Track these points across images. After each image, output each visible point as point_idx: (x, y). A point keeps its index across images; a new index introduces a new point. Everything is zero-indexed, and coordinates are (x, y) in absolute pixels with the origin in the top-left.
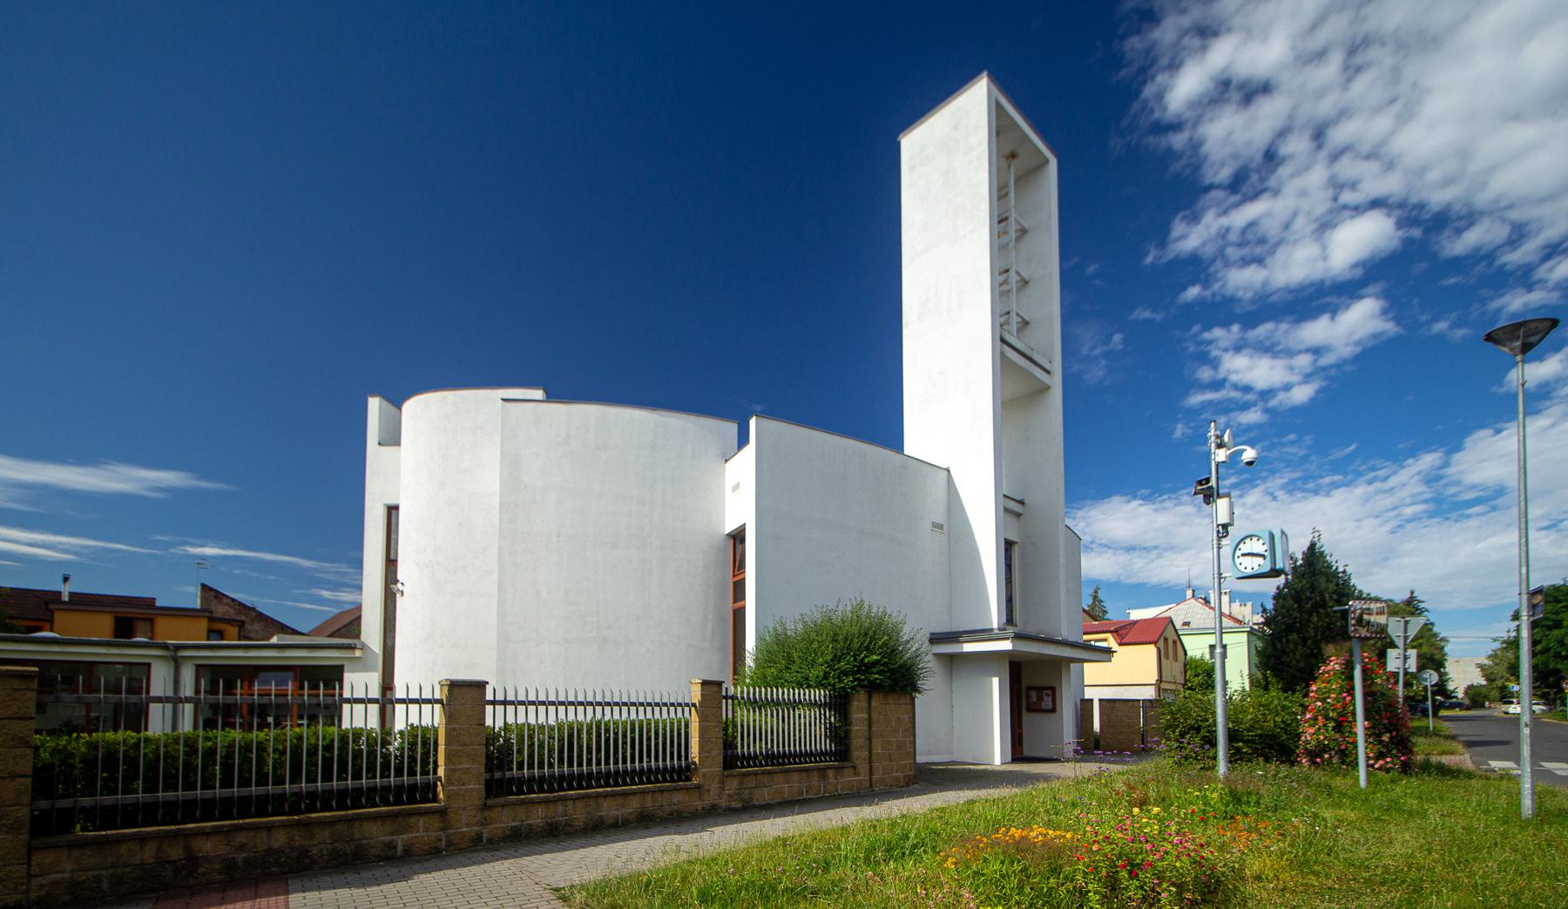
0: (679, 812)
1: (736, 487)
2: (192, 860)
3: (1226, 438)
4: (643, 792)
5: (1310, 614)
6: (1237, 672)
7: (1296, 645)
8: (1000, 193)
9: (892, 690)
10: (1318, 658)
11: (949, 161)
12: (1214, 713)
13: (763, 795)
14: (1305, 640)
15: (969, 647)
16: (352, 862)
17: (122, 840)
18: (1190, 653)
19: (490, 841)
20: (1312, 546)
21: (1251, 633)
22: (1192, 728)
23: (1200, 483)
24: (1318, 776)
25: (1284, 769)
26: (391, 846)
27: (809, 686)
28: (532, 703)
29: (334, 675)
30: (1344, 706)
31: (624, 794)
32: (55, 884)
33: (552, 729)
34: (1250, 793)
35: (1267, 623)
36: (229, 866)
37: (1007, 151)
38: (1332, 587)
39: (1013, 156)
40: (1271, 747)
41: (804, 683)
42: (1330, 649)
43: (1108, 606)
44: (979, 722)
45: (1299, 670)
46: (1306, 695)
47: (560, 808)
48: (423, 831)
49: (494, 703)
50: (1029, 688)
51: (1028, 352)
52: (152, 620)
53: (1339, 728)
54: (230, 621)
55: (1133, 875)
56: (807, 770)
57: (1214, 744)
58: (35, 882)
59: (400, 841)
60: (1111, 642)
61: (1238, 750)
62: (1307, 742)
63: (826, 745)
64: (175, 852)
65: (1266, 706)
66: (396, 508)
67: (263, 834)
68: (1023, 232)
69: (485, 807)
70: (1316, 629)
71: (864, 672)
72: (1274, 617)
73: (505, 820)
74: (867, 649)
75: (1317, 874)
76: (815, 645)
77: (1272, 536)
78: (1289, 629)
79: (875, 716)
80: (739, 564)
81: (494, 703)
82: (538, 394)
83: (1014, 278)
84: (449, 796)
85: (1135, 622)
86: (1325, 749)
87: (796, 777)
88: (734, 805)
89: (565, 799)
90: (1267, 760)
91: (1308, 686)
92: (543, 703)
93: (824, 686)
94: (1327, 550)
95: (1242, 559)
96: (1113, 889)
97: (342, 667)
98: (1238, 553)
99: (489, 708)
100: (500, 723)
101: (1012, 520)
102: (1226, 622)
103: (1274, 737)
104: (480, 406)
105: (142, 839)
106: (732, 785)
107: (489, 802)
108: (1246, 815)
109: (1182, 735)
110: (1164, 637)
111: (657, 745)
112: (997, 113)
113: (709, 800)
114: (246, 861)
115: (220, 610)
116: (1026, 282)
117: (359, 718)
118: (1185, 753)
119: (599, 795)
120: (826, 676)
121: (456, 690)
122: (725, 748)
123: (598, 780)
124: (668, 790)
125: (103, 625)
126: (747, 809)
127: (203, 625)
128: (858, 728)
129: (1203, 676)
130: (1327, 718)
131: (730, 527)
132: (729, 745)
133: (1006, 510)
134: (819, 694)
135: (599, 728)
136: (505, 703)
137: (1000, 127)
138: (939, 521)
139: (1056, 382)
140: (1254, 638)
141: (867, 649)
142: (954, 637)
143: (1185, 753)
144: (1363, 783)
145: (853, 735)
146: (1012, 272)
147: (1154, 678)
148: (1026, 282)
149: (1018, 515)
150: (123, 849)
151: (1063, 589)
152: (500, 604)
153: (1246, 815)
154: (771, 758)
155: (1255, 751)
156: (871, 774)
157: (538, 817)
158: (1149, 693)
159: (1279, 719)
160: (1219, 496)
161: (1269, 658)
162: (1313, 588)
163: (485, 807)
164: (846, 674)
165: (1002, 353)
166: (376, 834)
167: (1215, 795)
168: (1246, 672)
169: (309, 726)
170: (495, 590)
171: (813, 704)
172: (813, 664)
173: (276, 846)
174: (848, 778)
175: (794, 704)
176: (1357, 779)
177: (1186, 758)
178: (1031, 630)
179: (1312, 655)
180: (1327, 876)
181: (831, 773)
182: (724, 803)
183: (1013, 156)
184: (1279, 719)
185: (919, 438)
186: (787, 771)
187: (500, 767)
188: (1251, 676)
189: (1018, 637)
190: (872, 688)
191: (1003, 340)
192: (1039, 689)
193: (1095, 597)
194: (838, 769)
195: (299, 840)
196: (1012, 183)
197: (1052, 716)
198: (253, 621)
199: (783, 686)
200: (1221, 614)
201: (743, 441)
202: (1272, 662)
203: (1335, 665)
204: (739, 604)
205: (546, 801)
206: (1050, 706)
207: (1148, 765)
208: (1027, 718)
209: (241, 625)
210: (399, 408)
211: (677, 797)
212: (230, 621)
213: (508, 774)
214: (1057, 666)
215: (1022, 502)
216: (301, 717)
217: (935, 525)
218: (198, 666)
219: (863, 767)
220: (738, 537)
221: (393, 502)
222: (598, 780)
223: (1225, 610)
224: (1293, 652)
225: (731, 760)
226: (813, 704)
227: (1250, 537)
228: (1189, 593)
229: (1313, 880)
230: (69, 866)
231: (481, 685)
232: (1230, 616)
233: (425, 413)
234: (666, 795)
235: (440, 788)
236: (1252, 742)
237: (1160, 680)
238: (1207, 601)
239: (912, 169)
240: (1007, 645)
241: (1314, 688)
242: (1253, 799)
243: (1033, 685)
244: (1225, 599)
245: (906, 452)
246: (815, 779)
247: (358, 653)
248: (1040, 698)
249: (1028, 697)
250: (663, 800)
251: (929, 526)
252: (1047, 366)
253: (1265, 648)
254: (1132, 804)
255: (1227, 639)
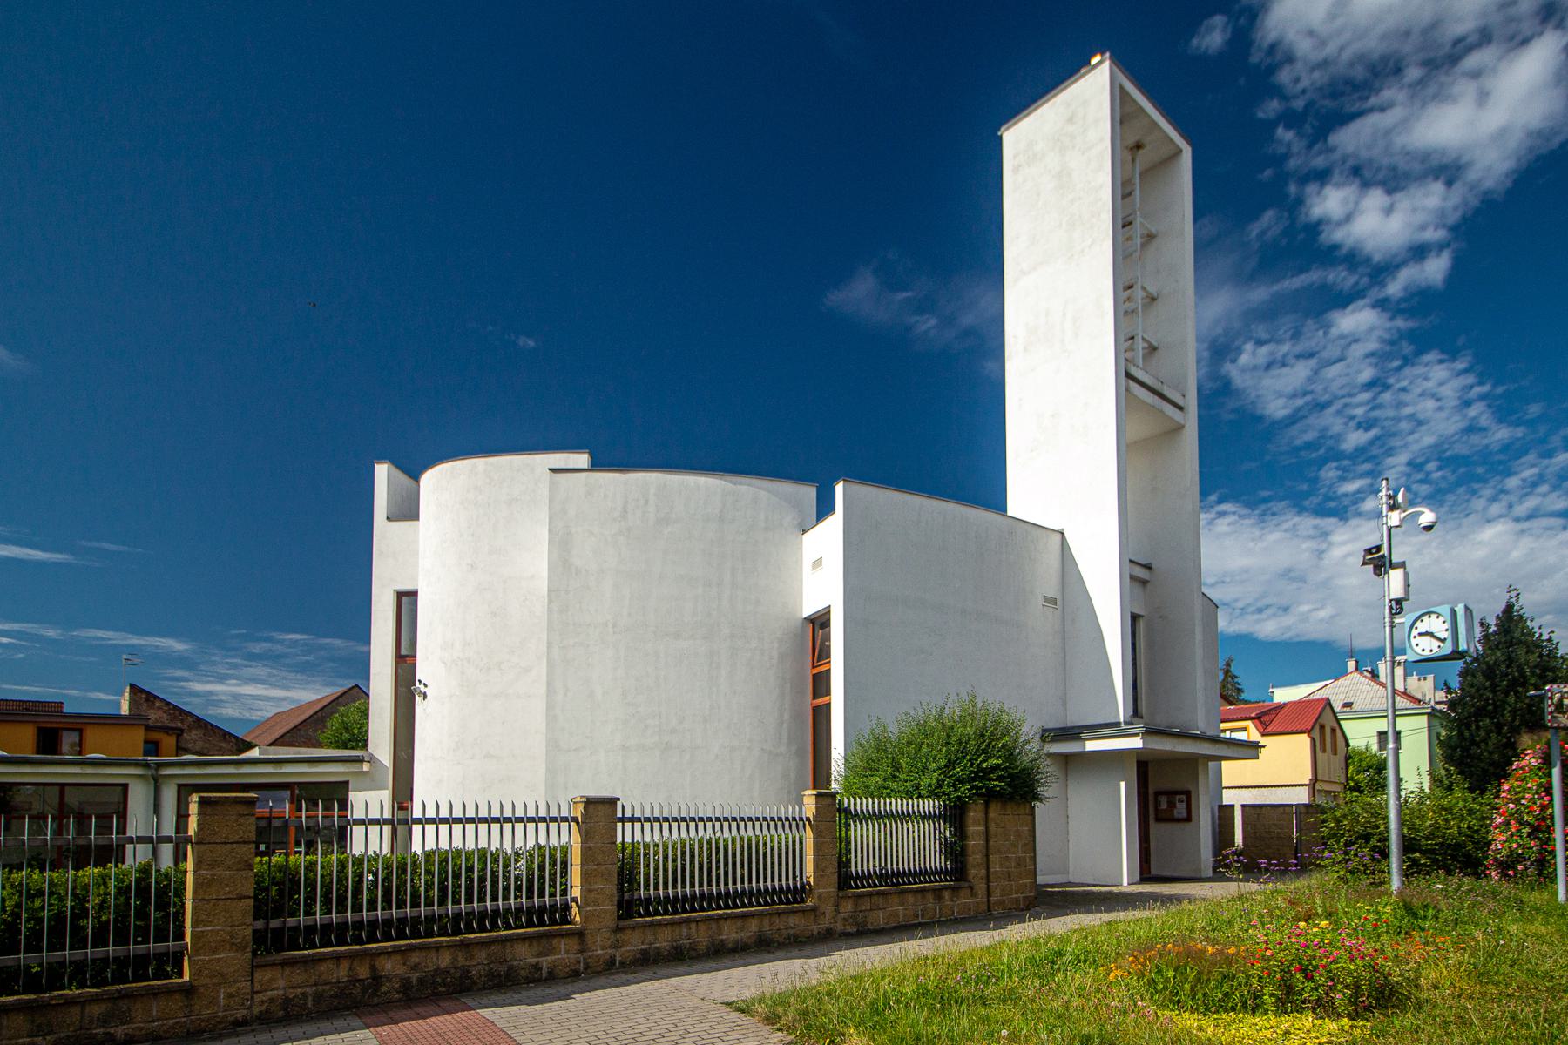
0: (796, 937)
1: (817, 563)
2: (377, 979)
3: (1400, 498)
4: (762, 914)
5: (1507, 695)
6: (1414, 766)
7: (1489, 732)
8: (1123, 191)
9: (1011, 798)
10: (1512, 750)
11: (1060, 162)
12: (1386, 818)
13: (878, 919)
14: (1499, 727)
15: (1091, 746)
16: (508, 982)
17: (322, 959)
18: (1352, 743)
19: (622, 964)
20: (1509, 608)
21: (1432, 715)
22: (1361, 837)
23: (1369, 551)
24: (1506, 888)
25: (1468, 883)
26: (537, 967)
27: (920, 796)
28: (508, 820)
29: (337, 793)
30: (1544, 808)
31: (744, 916)
32: (272, 1000)
33: (469, 856)
34: (1426, 907)
35: (1452, 704)
36: (406, 985)
37: (1131, 141)
38: (1533, 658)
39: (1138, 146)
40: (1454, 858)
41: (915, 792)
42: (1526, 740)
43: (1244, 680)
44: (1092, 831)
45: (1493, 764)
46: (1497, 797)
47: (685, 931)
48: (564, 953)
49: (622, 820)
50: (1158, 794)
51: (1157, 386)
52: (81, 731)
53: (1535, 831)
54: (166, 730)
55: (1309, 977)
56: (922, 891)
57: (1385, 855)
58: (258, 998)
59: (545, 962)
60: (1252, 733)
61: (1415, 862)
62: (1497, 851)
63: (940, 862)
64: (363, 972)
65: (1449, 810)
66: (413, 594)
67: (433, 954)
68: (1150, 237)
69: (618, 929)
70: (1514, 712)
71: (981, 779)
72: (1461, 699)
73: (635, 943)
74: (984, 752)
75: (1497, 984)
76: (925, 749)
77: (1454, 613)
78: (1480, 713)
79: (992, 828)
80: (821, 653)
81: (622, 820)
82: (582, 459)
83: (1139, 294)
84: (585, 918)
85: (1281, 706)
86: (1519, 859)
87: (910, 898)
88: (849, 929)
89: (688, 921)
90: (1449, 873)
91: (1500, 784)
92: (532, 820)
93: (939, 798)
94: (1527, 612)
95: (1420, 640)
96: (1288, 994)
97: (347, 783)
98: (1415, 632)
99: (417, 829)
100: (531, 843)
101: (1138, 589)
102: (1401, 702)
103: (1458, 846)
104: (524, 476)
105: (338, 958)
106: (847, 907)
107: (622, 924)
108: (1423, 930)
109: (1347, 844)
110: (1322, 725)
111: (692, 873)
112: (1120, 99)
113: (825, 923)
114: (420, 980)
115: (153, 715)
116: (1154, 299)
117: (367, 843)
118: (1350, 865)
119: (720, 917)
120: (940, 786)
121: (591, 807)
122: (620, 889)
123: (517, 918)
124: (784, 912)
125: (25, 737)
126: (863, 933)
127: (139, 735)
128: (974, 843)
129: (1372, 773)
130: (1522, 823)
131: (809, 608)
132: (843, 864)
133: (1132, 578)
134: (930, 805)
135: (683, 846)
136: (633, 820)
137: (1124, 113)
138: (1052, 594)
139: (1191, 421)
140: (1436, 722)
141: (984, 752)
142: (1073, 733)
143: (1350, 865)
144: (1561, 897)
145: (970, 850)
146: (1138, 288)
147: (1306, 777)
148: (1154, 299)
149: (1144, 583)
150: (323, 967)
151: (1199, 673)
152: (550, 707)
153: (1423, 930)
154: (885, 877)
155: (1435, 862)
156: (989, 895)
157: (664, 940)
158: (1301, 796)
159: (1464, 825)
160: (1392, 566)
161: (1454, 749)
162: (1510, 661)
163: (618, 929)
164: (962, 781)
165: (1127, 389)
166: (524, 955)
167: (1388, 909)
168: (1425, 767)
169: (307, 854)
170: (543, 689)
171: (926, 817)
172: (925, 770)
173: (443, 966)
174: (965, 900)
175: (904, 817)
176: (1555, 893)
177: (1352, 872)
178: (1161, 721)
179: (1506, 746)
180: (1508, 985)
181: (946, 894)
182: (839, 927)
183: (1138, 146)
184: (1464, 825)
185: (1027, 494)
186: (903, 892)
187: (278, 912)
188: (1432, 773)
189: (1150, 732)
190: (990, 796)
191: (1128, 375)
192: (1171, 794)
193: (1227, 672)
194: (955, 890)
195: (461, 961)
196: (1137, 181)
197: (1187, 826)
198: (190, 728)
199: (889, 796)
200: (1394, 692)
201: (824, 508)
202: (1458, 753)
203: (1531, 760)
204: (820, 701)
205: (672, 924)
206: (1185, 815)
207: (1315, 879)
208: (1154, 828)
209: (179, 733)
210: (415, 476)
211: (793, 920)
212: (166, 730)
213: (291, 922)
214: (1192, 764)
215: (1148, 567)
216: (298, 844)
217: (1047, 599)
218: (179, 786)
219: (980, 887)
220: (820, 622)
221: (406, 586)
222: (517, 918)
223: (1399, 686)
224: (1485, 741)
225: (845, 880)
226: (926, 817)
227: (1429, 614)
228: (1351, 665)
229: (1492, 989)
230: (282, 983)
231: (612, 802)
232: (1405, 694)
233: (441, 483)
234: (783, 917)
235: (575, 910)
236: (1433, 852)
237: (1315, 780)
238: (1374, 675)
239: (1016, 169)
240: (1136, 743)
241: (1506, 787)
242: (1431, 912)
243: (1165, 789)
244: (1399, 671)
245: (1013, 509)
246: (930, 902)
247: (366, 767)
248: (1172, 805)
249: (1157, 803)
250: (779, 923)
251: (1041, 600)
252: (1180, 401)
253: (1449, 738)
254: (1297, 919)
255: (1402, 724)
